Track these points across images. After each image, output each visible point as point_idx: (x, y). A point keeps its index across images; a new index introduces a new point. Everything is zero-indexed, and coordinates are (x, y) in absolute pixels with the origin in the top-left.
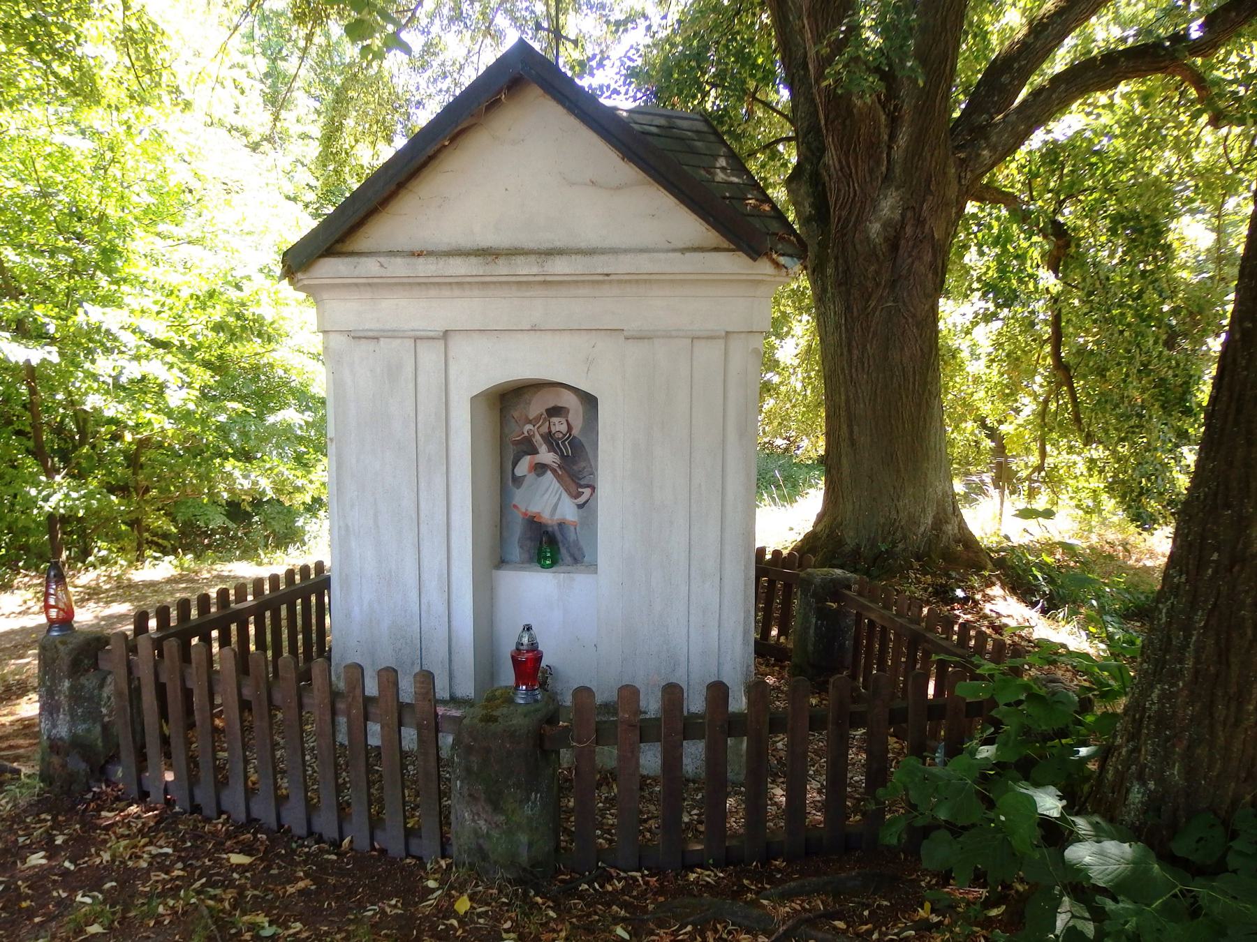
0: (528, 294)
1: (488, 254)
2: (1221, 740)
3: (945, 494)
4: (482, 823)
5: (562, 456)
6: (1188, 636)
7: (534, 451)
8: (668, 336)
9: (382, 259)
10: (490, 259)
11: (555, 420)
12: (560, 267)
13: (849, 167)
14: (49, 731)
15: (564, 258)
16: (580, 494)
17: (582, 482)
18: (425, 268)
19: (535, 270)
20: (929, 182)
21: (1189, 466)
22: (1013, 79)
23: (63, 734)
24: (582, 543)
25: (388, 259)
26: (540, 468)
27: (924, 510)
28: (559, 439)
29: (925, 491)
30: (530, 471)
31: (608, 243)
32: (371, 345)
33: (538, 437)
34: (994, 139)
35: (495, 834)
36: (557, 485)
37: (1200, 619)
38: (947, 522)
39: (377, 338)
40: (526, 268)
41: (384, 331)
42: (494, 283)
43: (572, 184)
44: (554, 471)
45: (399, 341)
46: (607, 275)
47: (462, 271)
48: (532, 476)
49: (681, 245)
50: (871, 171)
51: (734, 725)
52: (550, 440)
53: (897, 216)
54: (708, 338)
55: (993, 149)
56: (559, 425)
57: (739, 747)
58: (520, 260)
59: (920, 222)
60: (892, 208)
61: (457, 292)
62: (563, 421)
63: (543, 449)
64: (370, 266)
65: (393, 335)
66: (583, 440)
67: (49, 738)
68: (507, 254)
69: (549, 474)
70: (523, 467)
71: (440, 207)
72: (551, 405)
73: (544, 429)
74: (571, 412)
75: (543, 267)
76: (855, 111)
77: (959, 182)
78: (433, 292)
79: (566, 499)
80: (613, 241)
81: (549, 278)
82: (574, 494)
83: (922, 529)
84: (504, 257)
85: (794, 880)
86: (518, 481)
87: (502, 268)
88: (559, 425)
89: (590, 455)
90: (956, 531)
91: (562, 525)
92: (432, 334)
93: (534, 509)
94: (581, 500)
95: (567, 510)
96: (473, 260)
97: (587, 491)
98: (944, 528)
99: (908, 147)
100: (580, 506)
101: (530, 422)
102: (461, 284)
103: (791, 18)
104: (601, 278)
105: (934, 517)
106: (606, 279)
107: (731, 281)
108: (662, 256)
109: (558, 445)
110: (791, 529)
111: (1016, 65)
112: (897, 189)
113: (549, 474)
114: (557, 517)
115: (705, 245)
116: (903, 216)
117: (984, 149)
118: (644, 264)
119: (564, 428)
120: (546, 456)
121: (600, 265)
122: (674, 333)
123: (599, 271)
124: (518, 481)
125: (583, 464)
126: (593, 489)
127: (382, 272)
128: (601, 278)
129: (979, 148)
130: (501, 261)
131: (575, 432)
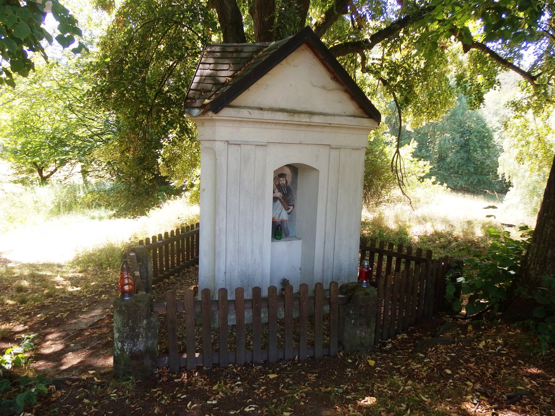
0: (299, 129)
1: (293, 112)
4: (363, 333)
5: (283, 194)
8: (345, 148)
9: (250, 110)
10: (292, 114)
11: (281, 179)
12: (316, 119)
14: (131, 349)
15: (318, 116)
17: (290, 204)
18: (267, 115)
21: (38, 178)
23: (141, 349)
24: (289, 228)
25: (252, 110)
28: (282, 187)
31: (324, 111)
32: (237, 147)
35: (367, 336)
36: (281, 205)
40: (305, 119)
41: (243, 142)
42: (290, 124)
43: (314, 86)
44: (280, 200)
45: (249, 146)
46: (331, 124)
47: (281, 118)
49: (348, 114)
58: (303, 115)
61: (273, 126)
62: (284, 179)
64: (245, 113)
65: (247, 143)
66: (292, 187)
67: (130, 353)
71: (265, 89)
74: (287, 176)
75: (310, 119)
78: (263, 126)
80: (327, 110)
81: (311, 124)
82: (287, 208)
84: (297, 114)
87: (296, 118)
89: (293, 193)
91: (282, 221)
92: (263, 144)
96: (286, 114)
97: (291, 207)
100: (289, 214)
102: (277, 123)
104: (328, 125)
106: (330, 126)
107: (365, 129)
109: (282, 189)
110: (179, 218)
114: (280, 218)
115: (355, 114)
119: (284, 182)
121: (329, 120)
122: (347, 147)
123: (329, 122)
125: (291, 197)
126: (294, 206)
127: (250, 116)
128: (328, 125)
130: (296, 115)
131: (289, 184)
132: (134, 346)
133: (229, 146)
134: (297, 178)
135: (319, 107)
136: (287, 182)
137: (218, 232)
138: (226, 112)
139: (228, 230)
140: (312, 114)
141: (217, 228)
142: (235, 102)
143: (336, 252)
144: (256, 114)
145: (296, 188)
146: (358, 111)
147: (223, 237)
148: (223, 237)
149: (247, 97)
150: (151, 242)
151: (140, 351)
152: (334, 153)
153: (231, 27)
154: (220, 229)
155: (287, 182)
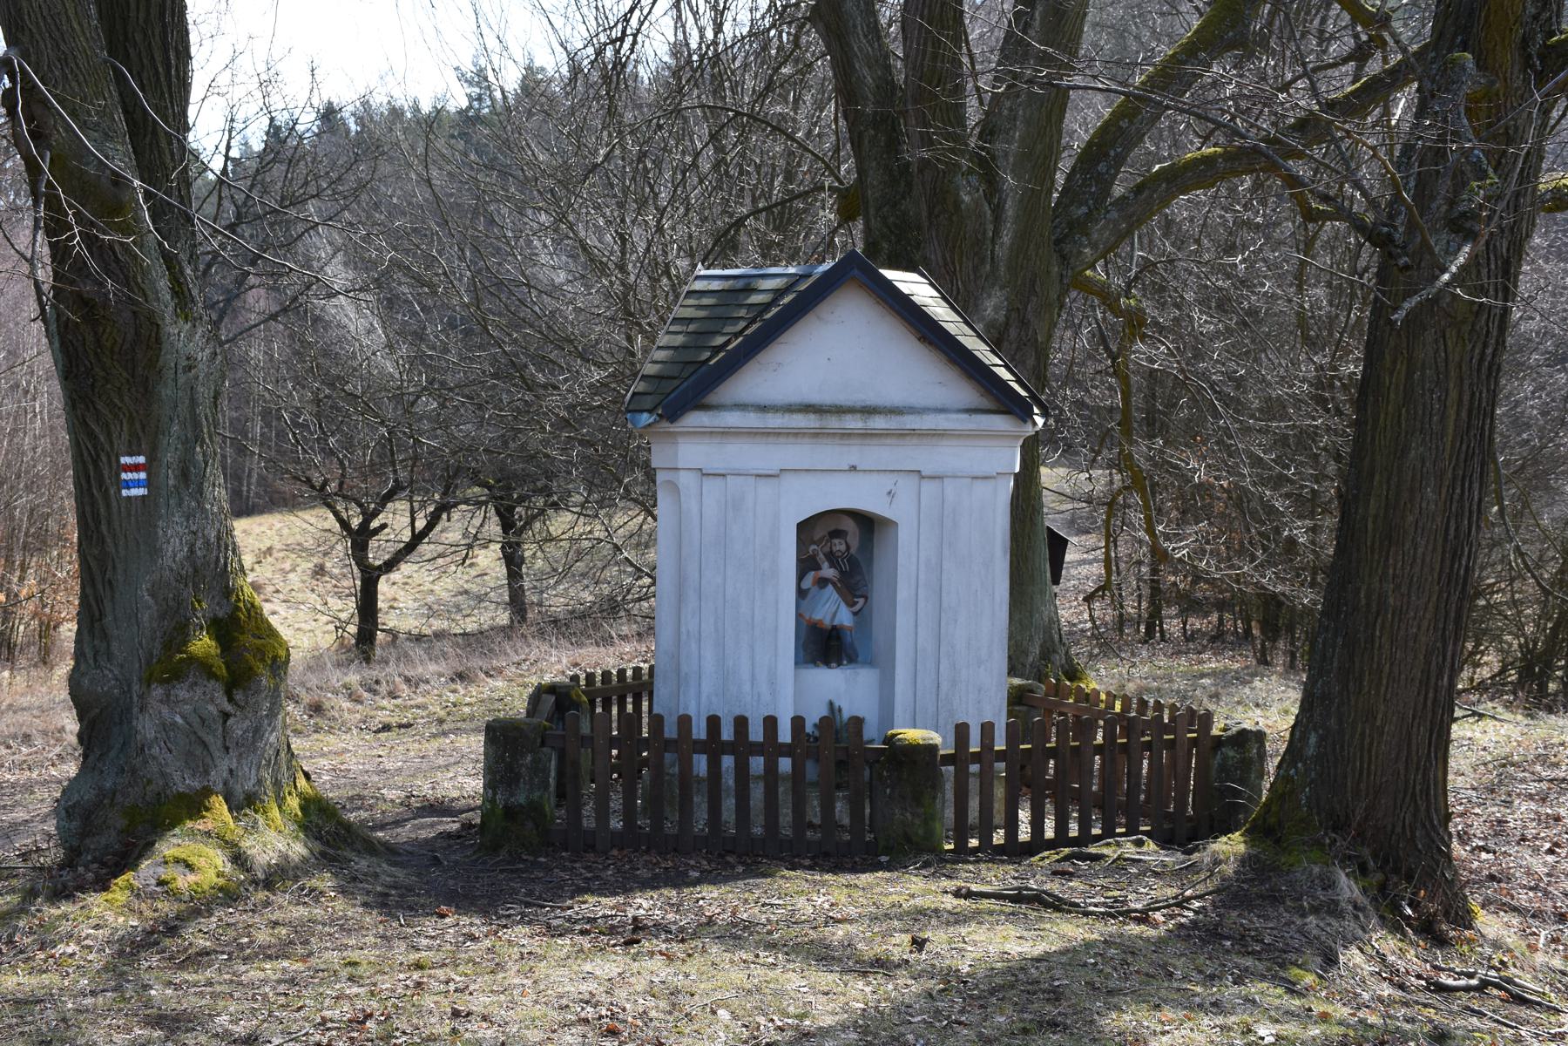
2: (1353, 703)
3: (1051, 621)
4: (908, 814)
5: (841, 572)
6: (1334, 651)
7: (818, 568)
11: (836, 541)
12: (879, 423)
13: (953, 263)
16: (855, 603)
19: (860, 425)
20: (1033, 283)
22: (1109, 168)
26: (822, 582)
27: (1031, 638)
29: (1031, 616)
30: (814, 584)
32: (719, 480)
33: (821, 556)
34: (1095, 236)
37: (1340, 641)
38: (1055, 651)
39: (724, 475)
40: (853, 423)
44: (834, 584)
47: (802, 425)
48: (815, 589)
49: (962, 406)
50: (976, 269)
52: (832, 558)
53: (1001, 316)
54: (749, 433)
55: (1094, 246)
56: (839, 546)
58: (848, 417)
59: (1024, 323)
60: (996, 309)
61: (791, 440)
63: (826, 565)
64: (732, 419)
67: (505, 807)
68: (838, 412)
69: (830, 587)
70: (808, 582)
72: (833, 528)
73: (827, 549)
76: (963, 206)
77: (1061, 280)
78: (771, 439)
79: (843, 608)
83: (1031, 659)
87: (833, 422)
88: (839, 546)
90: (1064, 661)
92: (770, 472)
93: (817, 616)
94: (857, 607)
95: (845, 617)
97: (861, 601)
99: (1012, 244)
100: (855, 614)
101: (814, 543)
102: (796, 434)
103: (857, 66)
105: (1041, 646)
108: (954, 416)
111: (1112, 153)
112: (1002, 288)
113: (830, 587)
116: (1007, 317)
117: (1085, 247)
119: (843, 548)
120: (828, 572)
126: (866, 598)
129: (1081, 245)
131: (853, 551)
132: (512, 795)
133: (704, 478)
134: (871, 540)
135: (892, 394)
136: (848, 547)
137: (684, 637)
138: (695, 419)
139: (703, 635)
140: (869, 411)
141: (683, 629)
142: (712, 398)
143: (942, 696)
144: (752, 420)
145: (870, 560)
146: (985, 403)
147: (694, 646)
148: (694, 646)
149: (762, 380)
150: (599, 684)
151: (521, 805)
152: (929, 487)
153: (872, 132)
154: (688, 632)
155: (848, 547)
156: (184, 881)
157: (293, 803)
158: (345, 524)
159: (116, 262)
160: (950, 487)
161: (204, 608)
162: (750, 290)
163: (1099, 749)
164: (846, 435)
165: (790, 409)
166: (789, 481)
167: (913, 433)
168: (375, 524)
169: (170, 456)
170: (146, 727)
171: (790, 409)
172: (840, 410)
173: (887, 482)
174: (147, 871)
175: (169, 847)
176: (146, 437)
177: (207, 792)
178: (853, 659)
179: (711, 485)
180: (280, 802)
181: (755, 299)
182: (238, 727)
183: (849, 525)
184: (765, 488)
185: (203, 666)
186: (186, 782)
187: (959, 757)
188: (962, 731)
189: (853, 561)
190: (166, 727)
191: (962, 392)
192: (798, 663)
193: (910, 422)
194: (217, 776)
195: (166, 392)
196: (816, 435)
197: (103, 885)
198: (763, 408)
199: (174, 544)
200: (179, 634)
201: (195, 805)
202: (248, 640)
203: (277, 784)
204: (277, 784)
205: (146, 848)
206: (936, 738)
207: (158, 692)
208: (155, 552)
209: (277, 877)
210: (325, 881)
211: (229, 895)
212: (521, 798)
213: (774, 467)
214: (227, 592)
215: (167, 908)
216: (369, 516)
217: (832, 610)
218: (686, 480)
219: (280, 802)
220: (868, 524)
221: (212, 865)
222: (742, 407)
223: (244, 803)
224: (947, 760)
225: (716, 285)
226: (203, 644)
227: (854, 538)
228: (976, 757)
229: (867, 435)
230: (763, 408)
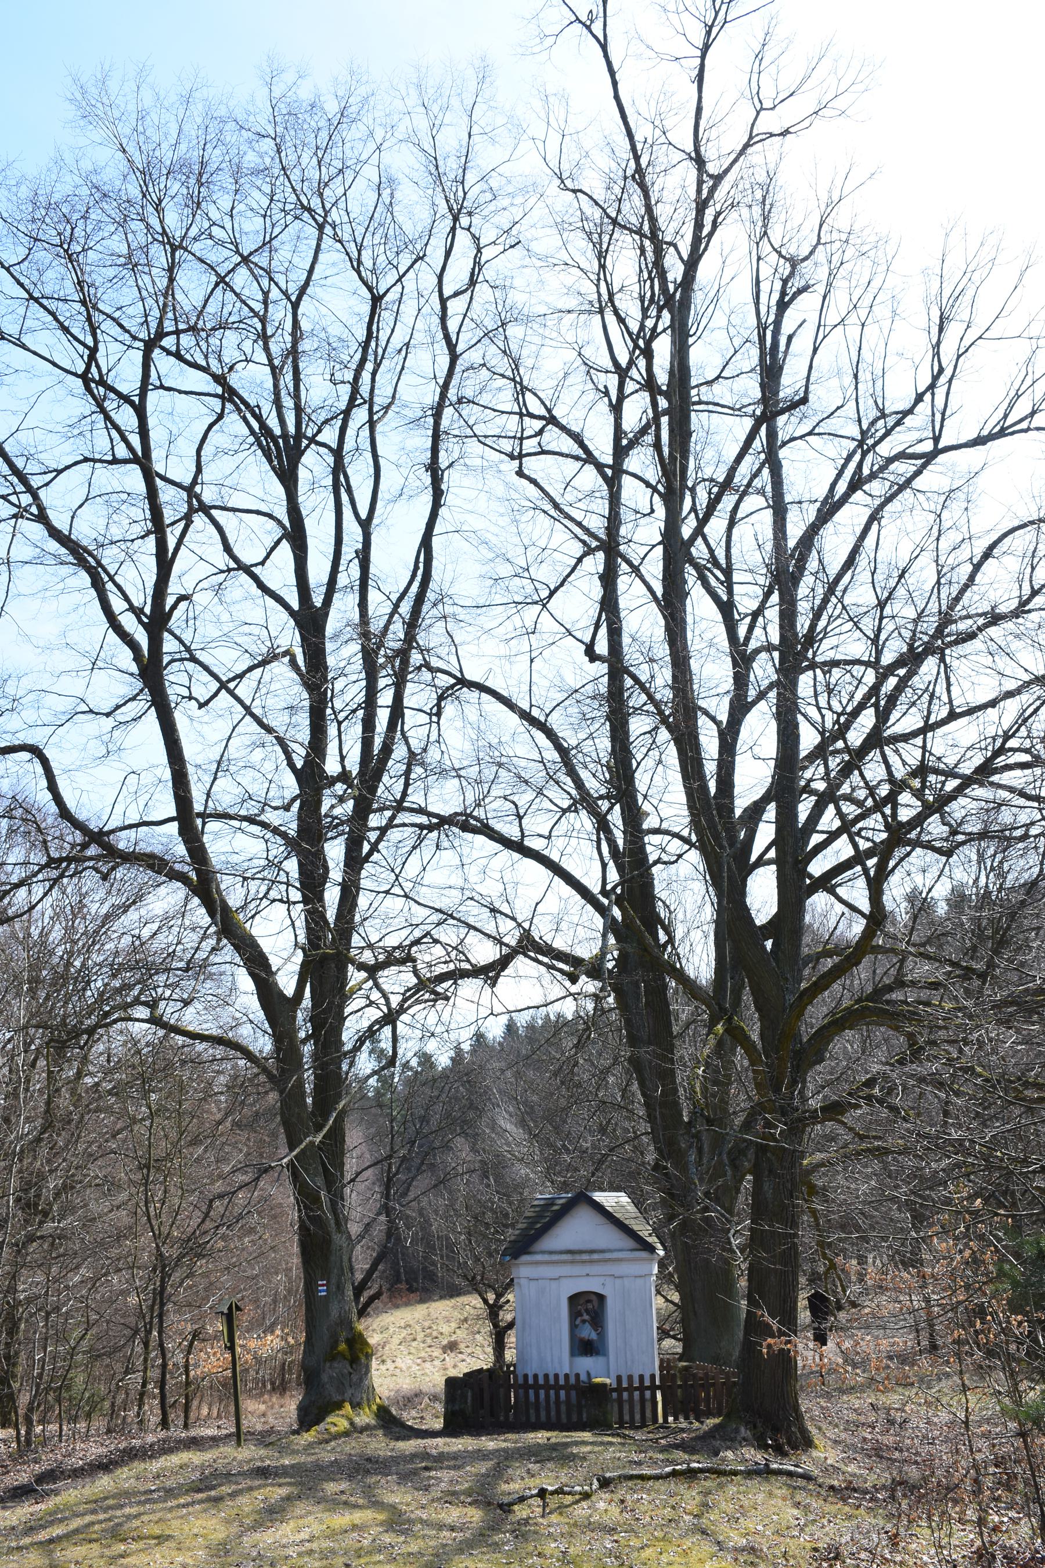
12: (595, 1256)
18: (555, 1257)
26: (584, 1321)
40: (585, 1257)
51: (542, 1387)
52: (587, 1311)
56: (590, 1306)
57: (637, 1394)
64: (539, 1257)
70: (578, 1322)
80: (611, 1246)
85: (909, 1273)
86: (576, 1326)
87: (577, 1257)
88: (590, 1306)
95: (594, 1336)
98: (570, 1017)
118: (620, 1255)
120: (586, 1317)
124: (576, 1326)
135: (602, 1244)
138: (525, 1258)
140: (592, 1252)
146: (638, 1246)
152: (618, 1281)
156: (333, 1429)
157: (375, 1407)
158: (485, 1301)
159: (318, 1221)
160: (626, 1280)
161: (343, 1335)
162: (553, 1204)
163: (680, 1386)
164: (584, 1262)
165: (561, 1252)
166: (563, 1281)
167: (609, 1260)
168: (503, 1300)
169: (334, 1281)
170: (325, 1378)
171: (561, 1252)
172: (581, 1252)
173: (602, 1280)
174: (322, 1426)
175: (329, 1419)
176: (326, 1275)
177: (344, 1401)
178: (598, 1353)
179: (532, 1283)
180: (369, 1407)
181: (555, 1208)
182: (355, 1378)
183: (594, 1298)
184: (554, 1284)
185: (341, 1354)
186: (337, 1398)
187: (619, 1389)
188: (619, 1378)
189: (596, 1313)
190: (331, 1378)
191: (630, 1243)
192: (573, 1354)
193: (608, 1256)
194: (347, 1395)
195: (333, 1258)
196: (572, 1262)
197: (308, 1430)
198: (551, 1253)
199: (334, 1313)
200: (335, 1344)
201: (339, 1406)
202: (358, 1346)
203: (368, 1400)
204: (368, 1400)
205: (323, 1419)
206: (608, 1381)
207: (328, 1365)
208: (329, 1315)
209: (367, 1428)
210: (380, 1432)
211: (346, 1434)
212: (457, 1407)
213: (557, 1275)
214: (352, 1329)
215: (326, 1436)
216: (499, 1296)
217: (587, 1332)
218: (523, 1282)
219: (369, 1407)
220: (601, 1298)
221: (343, 1424)
222: (543, 1252)
223: (356, 1405)
224: (614, 1390)
225: (542, 1202)
226: (343, 1347)
227: (596, 1303)
228: (626, 1389)
229: (591, 1262)
230: (551, 1253)
